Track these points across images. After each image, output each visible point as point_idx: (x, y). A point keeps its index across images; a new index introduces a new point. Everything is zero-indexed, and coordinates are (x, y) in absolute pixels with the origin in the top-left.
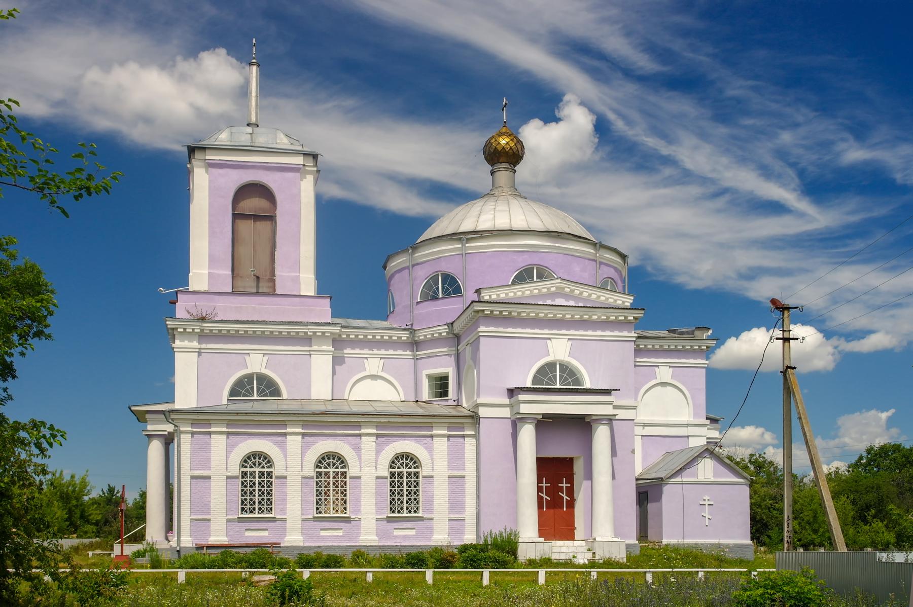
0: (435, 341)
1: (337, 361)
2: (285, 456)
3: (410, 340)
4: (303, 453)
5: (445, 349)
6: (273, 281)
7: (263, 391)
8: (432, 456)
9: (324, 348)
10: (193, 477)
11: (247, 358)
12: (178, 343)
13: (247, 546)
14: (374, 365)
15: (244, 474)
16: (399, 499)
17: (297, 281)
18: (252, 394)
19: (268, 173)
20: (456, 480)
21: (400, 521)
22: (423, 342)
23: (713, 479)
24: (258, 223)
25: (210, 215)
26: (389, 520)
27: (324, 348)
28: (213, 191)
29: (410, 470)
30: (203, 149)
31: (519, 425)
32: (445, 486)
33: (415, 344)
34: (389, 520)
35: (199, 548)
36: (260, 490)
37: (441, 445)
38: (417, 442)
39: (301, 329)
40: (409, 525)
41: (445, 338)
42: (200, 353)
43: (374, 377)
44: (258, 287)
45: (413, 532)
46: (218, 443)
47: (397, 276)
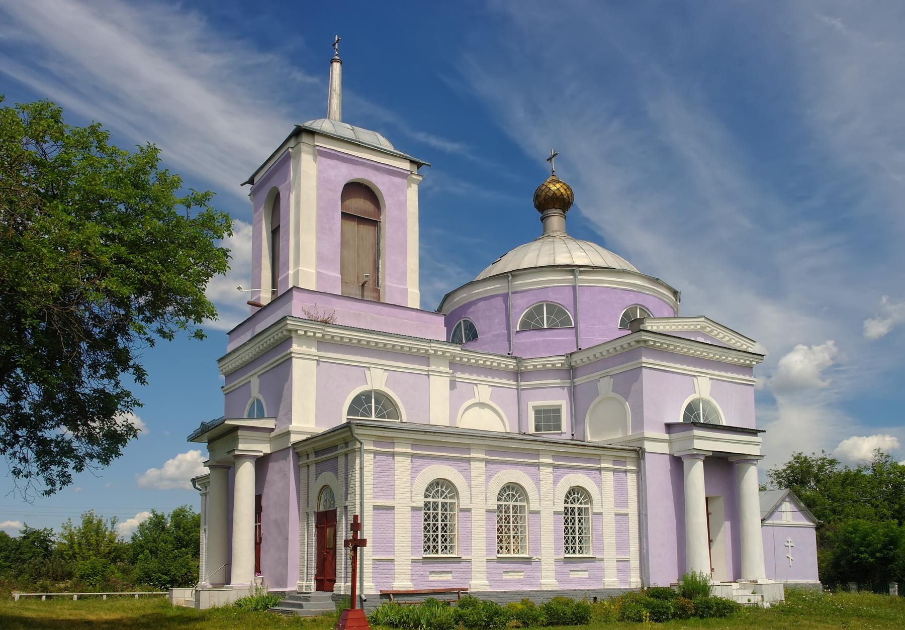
0: (545, 372)
1: (453, 385)
3: (516, 369)
4: (413, 478)
5: (558, 381)
6: (378, 292)
7: (365, 410)
8: (601, 491)
9: (442, 369)
10: (376, 508)
12: (295, 347)
14: (484, 393)
17: (404, 292)
18: (371, 416)
19: (377, 173)
20: (622, 516)
21: (575, 562)
22: (530, 372)
23: (792, 522)
24: (361, 226)
25: (319, 208)
26: (567, 560)
27: (442, 369)
28: (323, 182)
31: (686, 462)
32: (613, 525)
33: (518, 375)
34: (567, 560)
35: (385, 595)
37: (607, 477)
39: (423, 346)
40: (582, 566)
41: (559, 370)
42: (318, 361)
43: (482, 405)
44: (363, 295)
45: (585, 575)
46: (402, 465)
47: (481, 304)
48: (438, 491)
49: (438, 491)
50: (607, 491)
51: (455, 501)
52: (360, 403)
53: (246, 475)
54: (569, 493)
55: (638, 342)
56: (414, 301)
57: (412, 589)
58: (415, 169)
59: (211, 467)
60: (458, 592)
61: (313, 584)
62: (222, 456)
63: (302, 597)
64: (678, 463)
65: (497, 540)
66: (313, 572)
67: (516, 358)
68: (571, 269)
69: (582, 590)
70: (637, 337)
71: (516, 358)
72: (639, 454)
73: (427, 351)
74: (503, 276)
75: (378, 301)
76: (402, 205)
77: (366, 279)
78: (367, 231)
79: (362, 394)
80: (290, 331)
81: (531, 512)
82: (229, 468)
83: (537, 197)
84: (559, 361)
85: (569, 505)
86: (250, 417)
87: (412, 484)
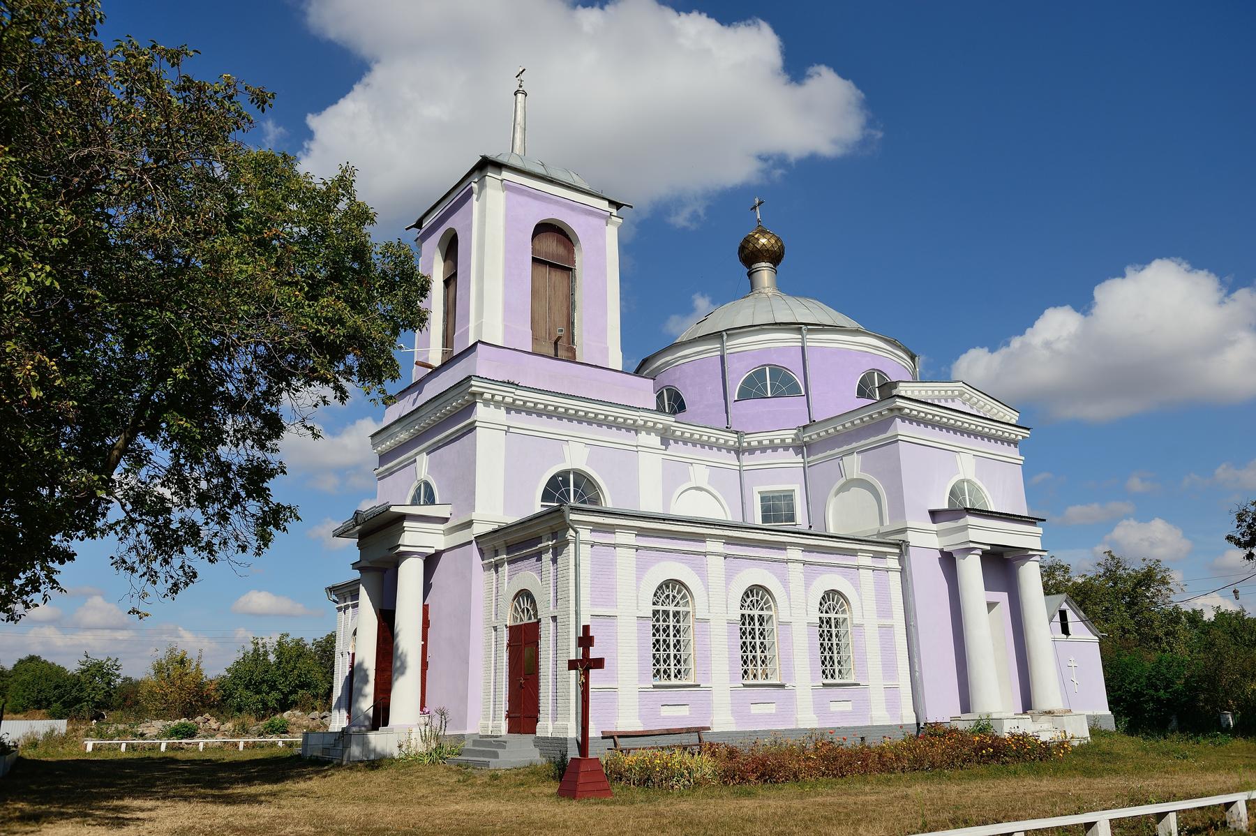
2: (707, 589)
4: (639, 579)
7: (562, 494)
8: (860, 595)
11: (565, 447)
13: (669, 732)
15: (655, 613)
16: (665, 641)
17: (605, 352)
20: (886, 630)
24: (553, 273)
25: (507, 251)
28: (511, 222)
29: (677, 609)
30: (499, 166)
33: (739, 451)
36: (668, 635)
38: (844, 576)
44: (556, 355)
45: (847, 707)
46: (625, 560)
48: (668, 596)
49: (668, 596)
50: (869, 593)
51: (690, 609)
52: (556, 488)
53: (410, 574)
54: (823, 598)
55: (891, 410)
56: (615, 359)
57: (641, 729)
58: (614, 211)
59: (362, 569)
60: (698, 730)
61: (504, 726)
62: (379, 553)
63: (490, 744)
64: (948, 561)
65: (653, 661)
66: (504, 706)
67: (737, 433)
68: (795, 327)
69: (846, 728)
70: (888, 404)
71: (737, 433)
72: (902, 547)
73: (635, 421)
74: (717, 336)
75: (572, 360)
76: (602, 250)
77: (559, 334)
78: (557, 276)
79: (554, 478)
80: (474, 394)
81: (781, 623)
82: (384, 571)
83: (742, 248)
84: (789, 436)
85: (824, 615)
86: (415, 502)
87: (638, 588)
